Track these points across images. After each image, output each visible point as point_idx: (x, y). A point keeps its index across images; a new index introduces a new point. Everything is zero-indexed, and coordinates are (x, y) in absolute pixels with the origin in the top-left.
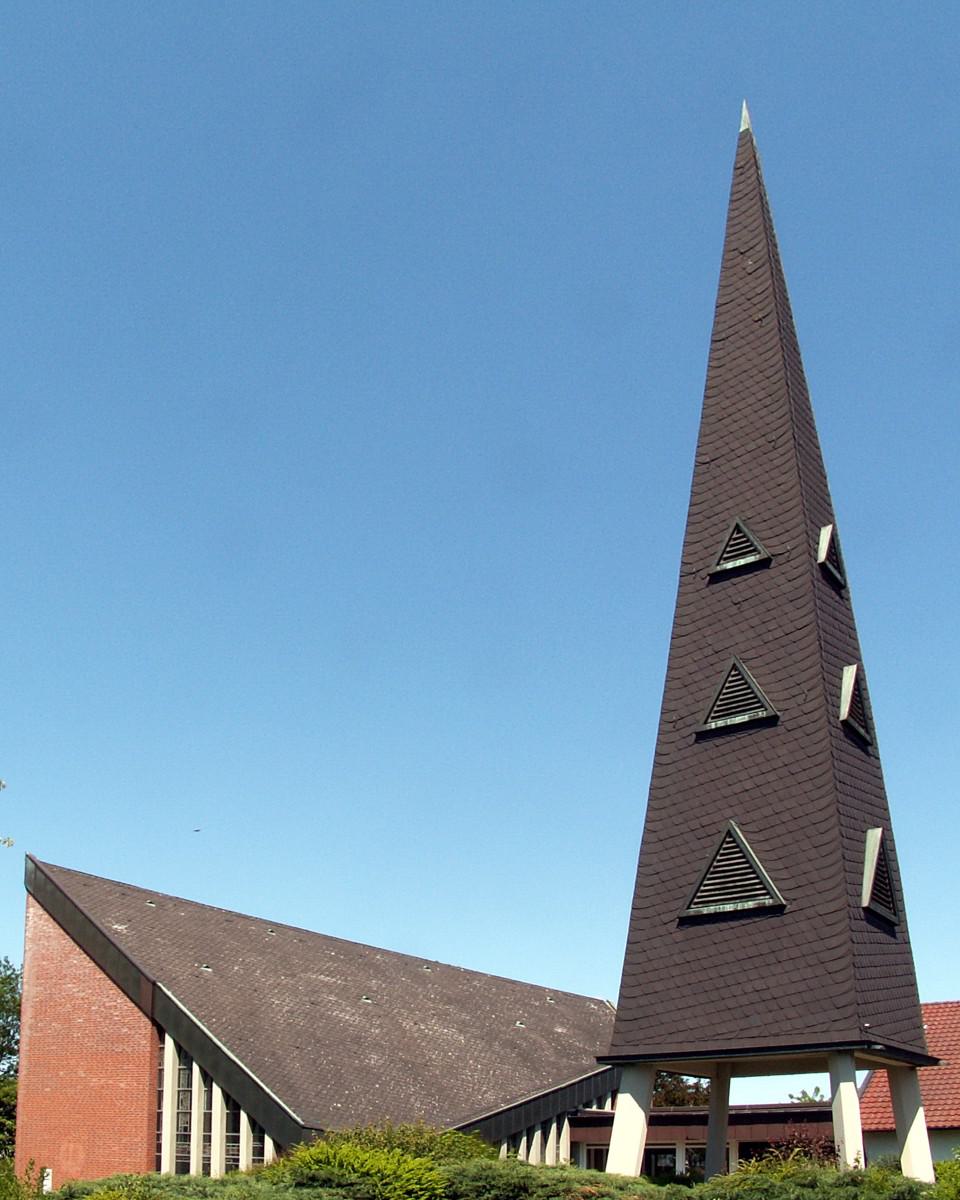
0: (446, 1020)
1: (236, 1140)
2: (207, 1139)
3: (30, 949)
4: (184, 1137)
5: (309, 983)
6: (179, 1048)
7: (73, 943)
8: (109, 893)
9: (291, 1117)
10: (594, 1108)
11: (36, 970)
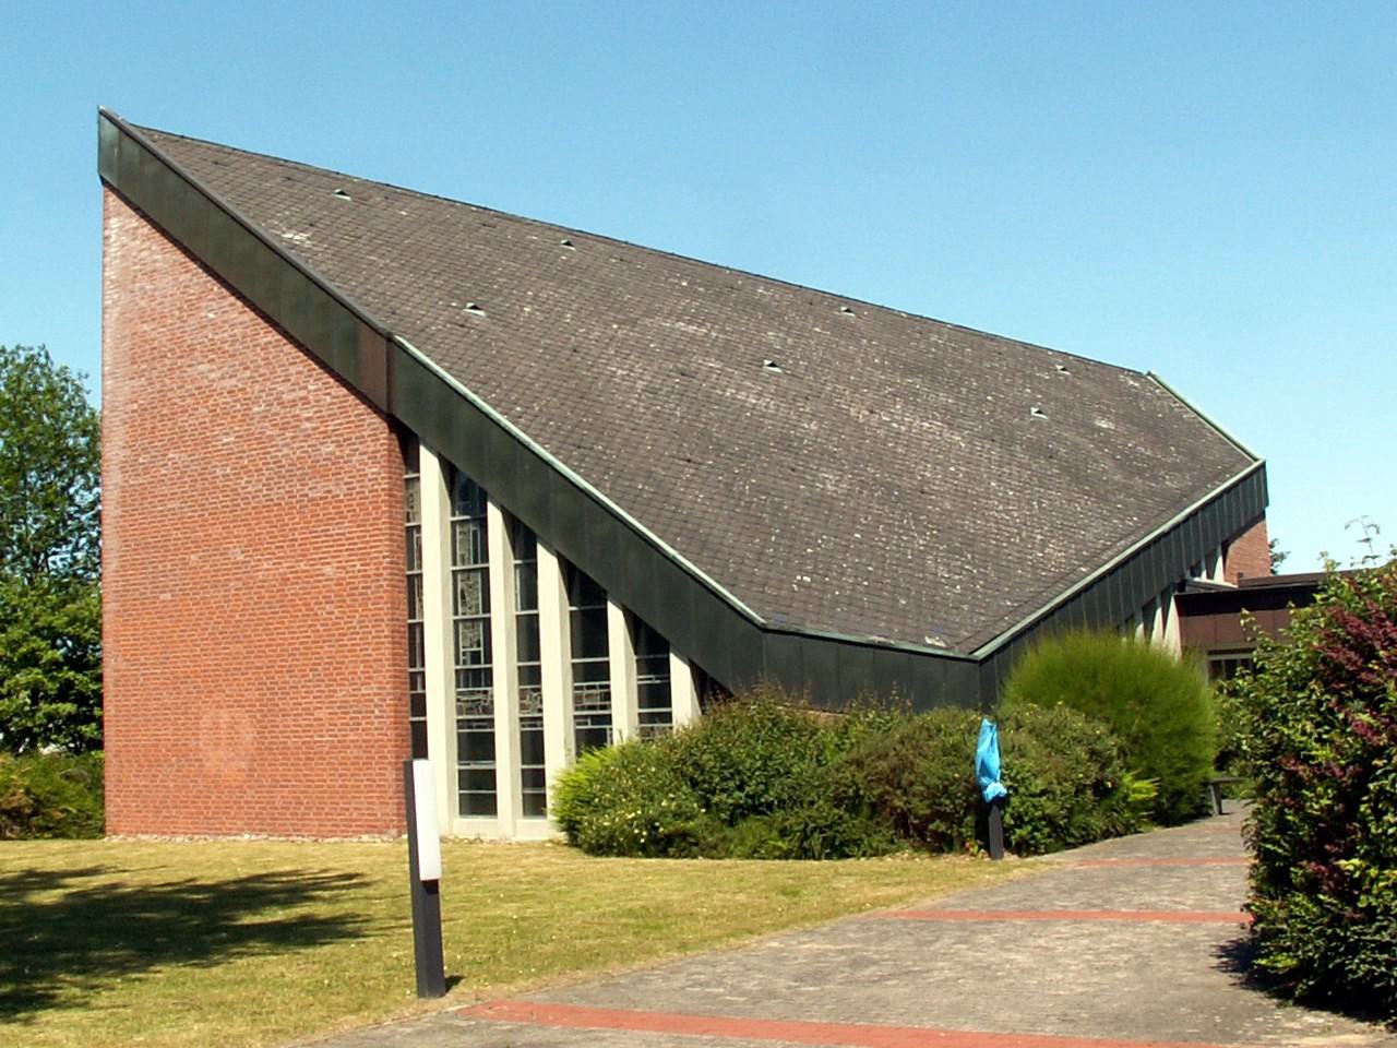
0: (916, 405)
1: (602, 672)
2: (531, 676)
3: (115, 303)
4: (474, 676)
5: (664, 336)
6: (450, 472)
7: (205, 277)
8: (262, 177)
9: (732, 607)
10: (1203, 578)
11: (128, 343)
